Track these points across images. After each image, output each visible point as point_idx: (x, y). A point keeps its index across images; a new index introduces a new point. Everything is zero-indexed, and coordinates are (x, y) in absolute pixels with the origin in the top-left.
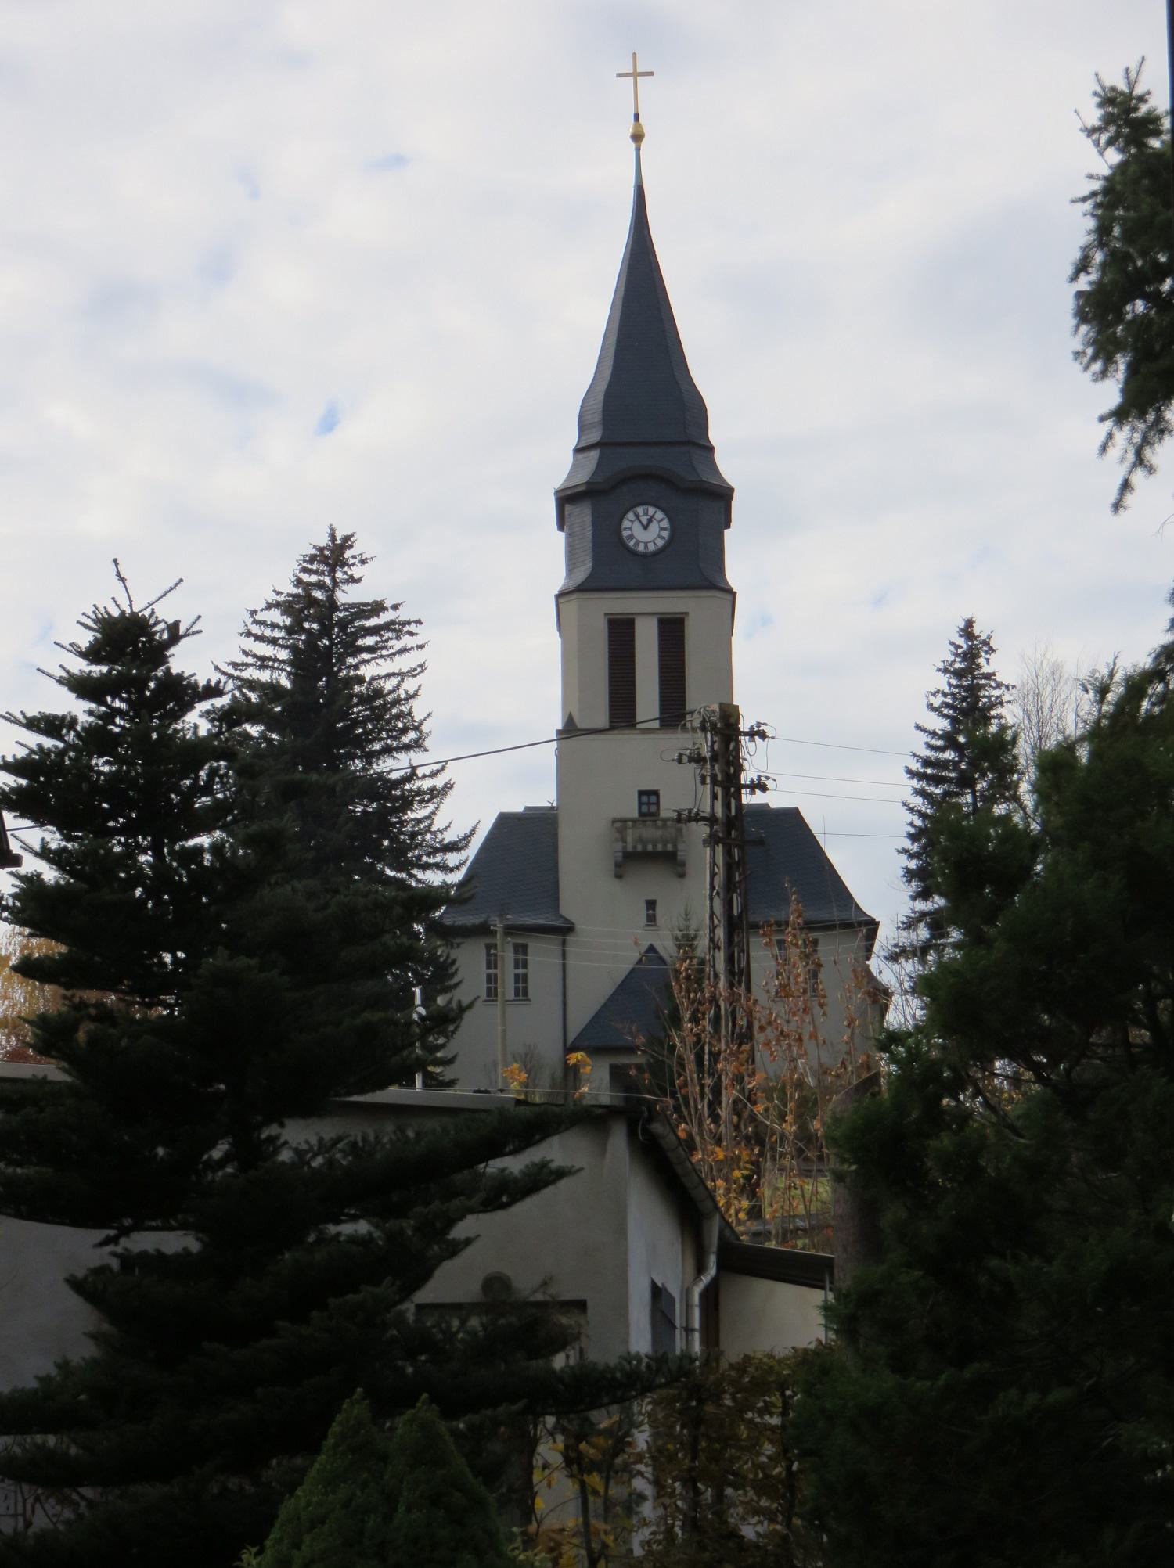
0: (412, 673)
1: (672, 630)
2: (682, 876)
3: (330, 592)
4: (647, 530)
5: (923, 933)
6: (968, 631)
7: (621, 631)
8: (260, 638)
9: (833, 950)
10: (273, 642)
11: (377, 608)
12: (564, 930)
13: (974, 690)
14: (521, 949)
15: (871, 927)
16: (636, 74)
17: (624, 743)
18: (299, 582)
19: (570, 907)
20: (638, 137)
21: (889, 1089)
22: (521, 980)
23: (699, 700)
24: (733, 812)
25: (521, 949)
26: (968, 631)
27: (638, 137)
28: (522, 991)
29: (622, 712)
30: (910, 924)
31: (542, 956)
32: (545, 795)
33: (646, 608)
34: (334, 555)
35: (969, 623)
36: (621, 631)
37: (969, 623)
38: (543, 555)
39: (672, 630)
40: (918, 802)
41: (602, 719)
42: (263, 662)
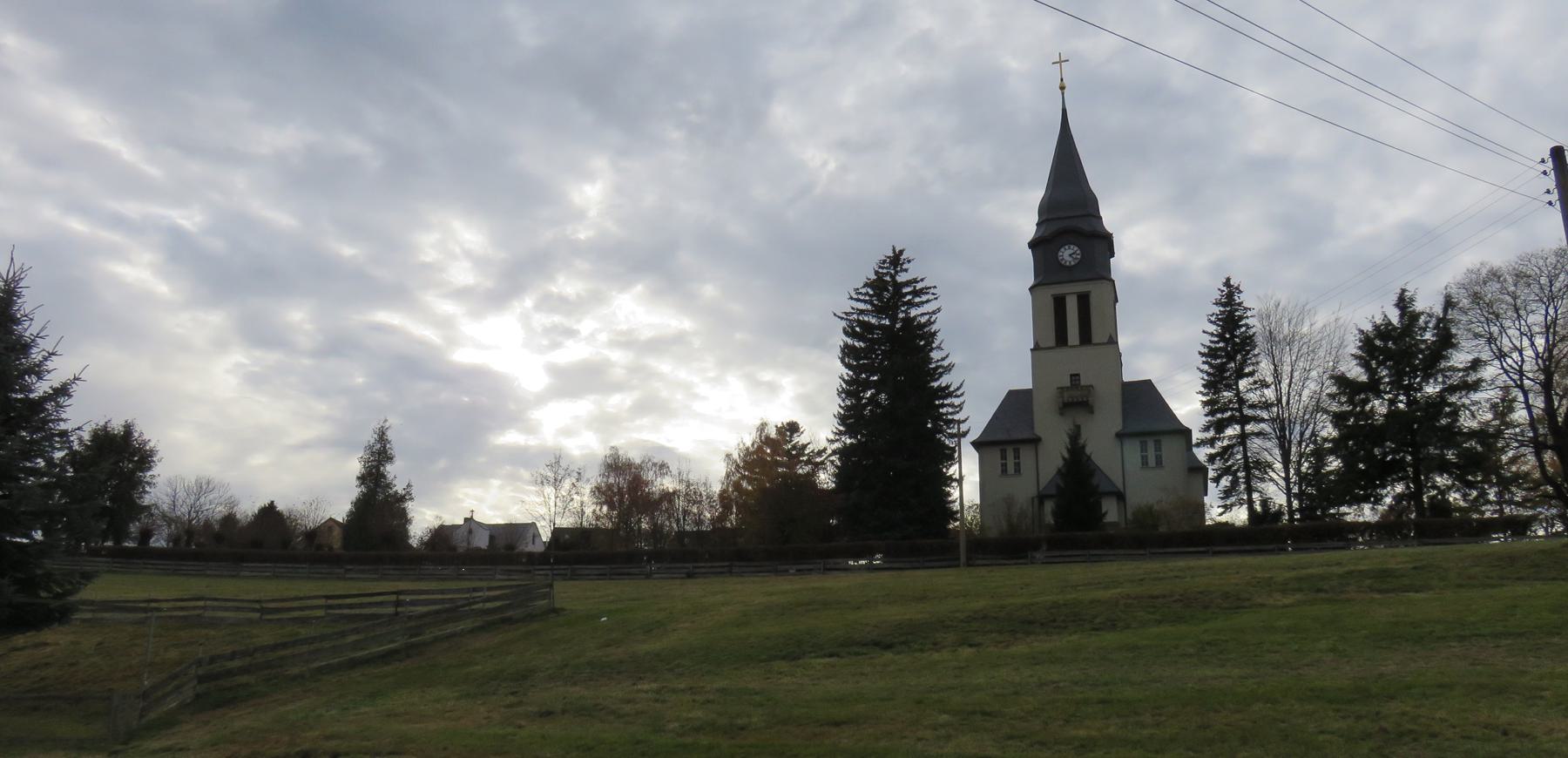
0: (934, 313)
1: (1084, 300)
2: (1092, 412)
3: (893, 277)
4: (1068, 254)
5: (1211, 434)
6: (1227, 283)
7: (1059, 303)
8: (858, 300)
9: (1170, 447)
10: (865, 302)
11: (916, 281)
12: (1035, 441)
13: (1231, 313)
14: (1017, 452)
15: (1187, 433)
16: (1060, 62)
17: (1062, 353)
18: (876, 273)
19: (1039, 430)
20: (1062, 88)
21: (380, 328)
22: (1017, 465)
23: (1098, 335)
24: (1258, 508)
25: (1017, 452)
26: (1227, 283)
27: (1062, 88)
28: (1018, 470)
29: (1061, 339)
30: (1207, 429)
31: (1027, 455)
32: (1026, 383)
33: (1071, 291)
34: (896, 260)
35: (1228, 279)
36: (1059, 303)
37: (1228, 279)
38: (1018, 274)
39: (1084, 300)
40: (1206, 367)
41: (1052, 343)
42: (862, 312)
